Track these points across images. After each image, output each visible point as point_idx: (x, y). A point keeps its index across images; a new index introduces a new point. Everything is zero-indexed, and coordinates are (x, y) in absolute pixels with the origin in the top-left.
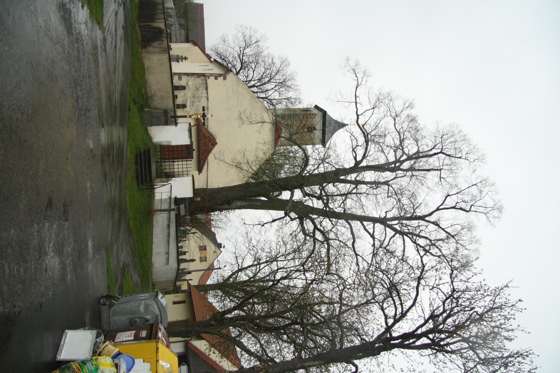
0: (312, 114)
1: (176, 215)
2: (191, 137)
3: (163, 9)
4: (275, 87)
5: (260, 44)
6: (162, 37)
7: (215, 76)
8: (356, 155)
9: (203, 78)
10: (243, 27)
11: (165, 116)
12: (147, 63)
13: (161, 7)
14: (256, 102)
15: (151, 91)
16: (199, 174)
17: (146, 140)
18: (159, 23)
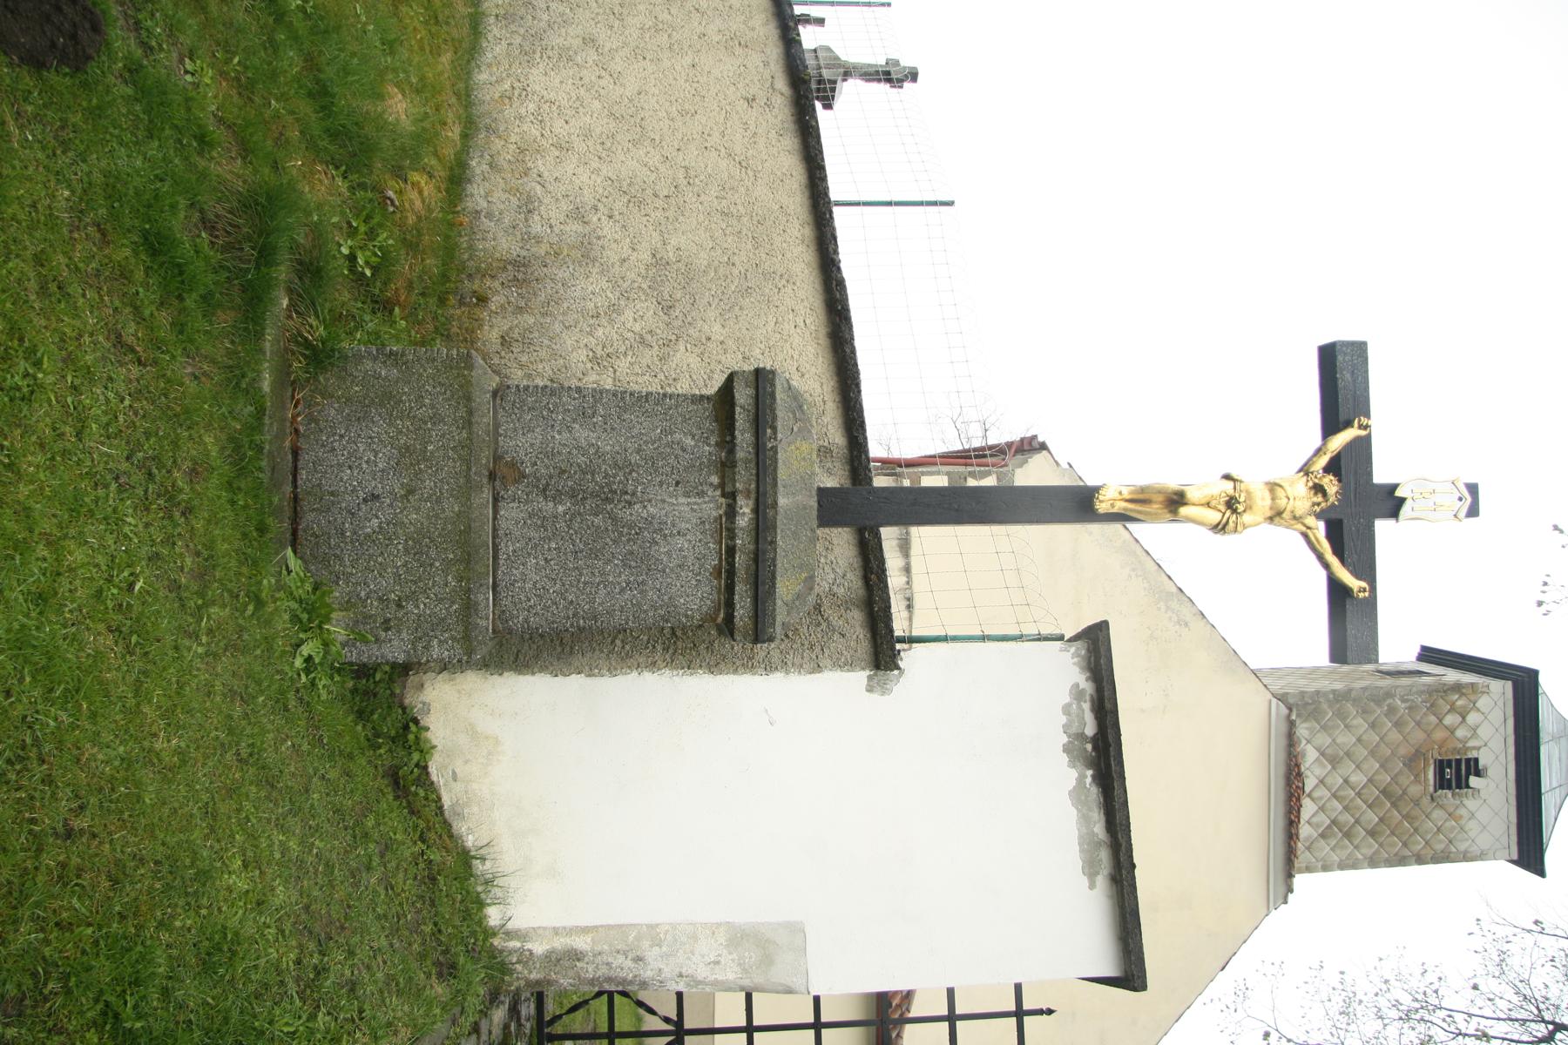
11: (726, 467)
14: (1178, 622)
15: (528, 206)
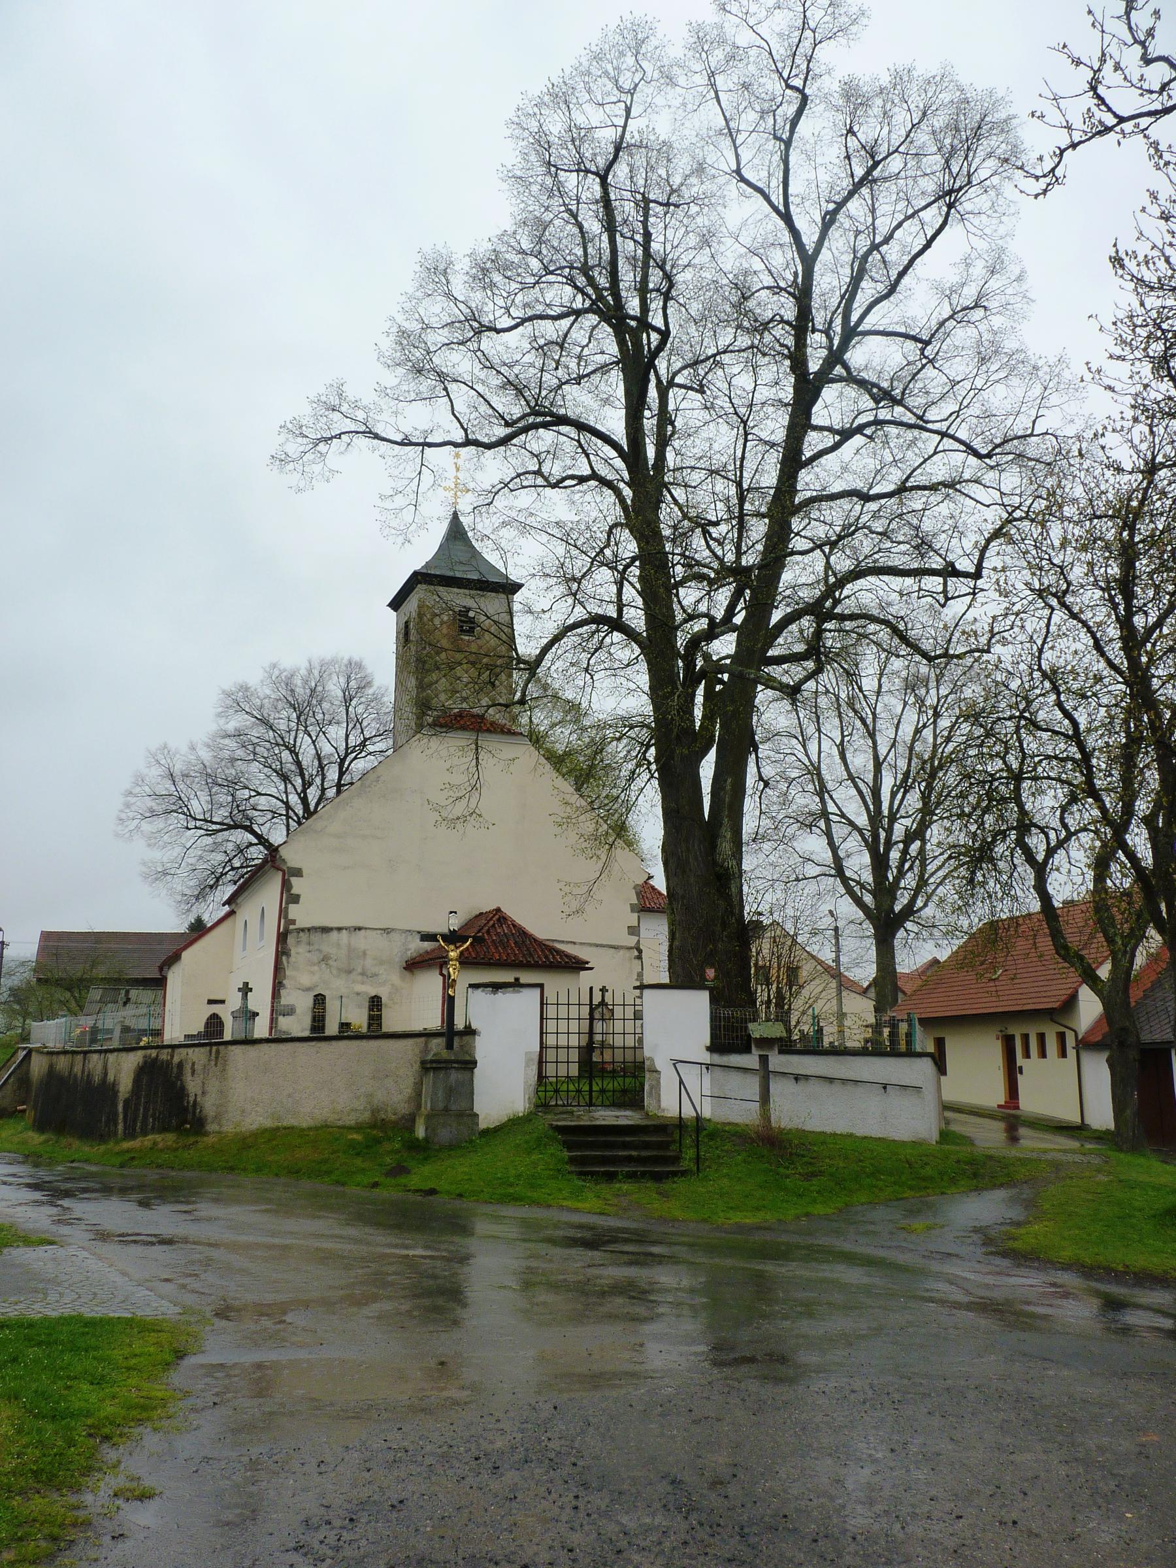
0: (420, 615)
1: (781, 1052)
2: (517, 985)
3: (69, 1056)
4: (310, 736)
5: (178, 768)
6: (169, 1063)
7: (287, 903)
8: (572, 477)
9: (291, 940)
10: (123, 816)
11: (446, 1068)
12: (256, 1120)
13: (62, 1063)
16: (591, 969)
17: (527, 1137)
18: (118, 1071)
